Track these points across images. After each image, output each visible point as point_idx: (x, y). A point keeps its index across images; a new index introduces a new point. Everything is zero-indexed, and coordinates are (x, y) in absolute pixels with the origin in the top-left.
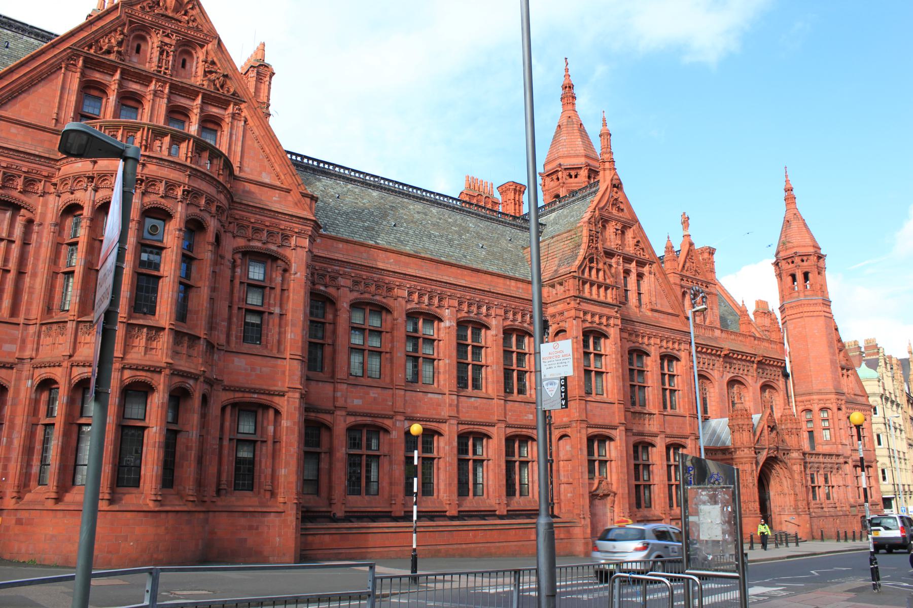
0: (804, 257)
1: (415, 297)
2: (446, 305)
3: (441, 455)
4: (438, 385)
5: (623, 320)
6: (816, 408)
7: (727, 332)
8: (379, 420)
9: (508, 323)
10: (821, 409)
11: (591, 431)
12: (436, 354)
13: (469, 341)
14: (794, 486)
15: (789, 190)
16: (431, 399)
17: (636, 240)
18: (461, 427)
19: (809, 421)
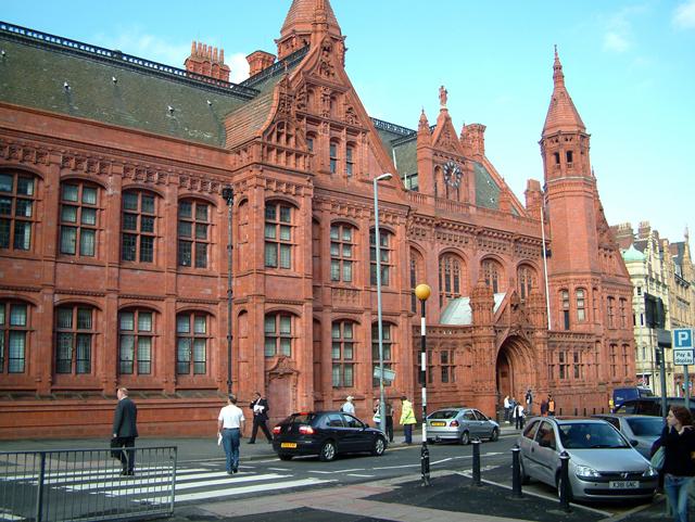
0: (568, 136)
1: (72, 163)
2: (109, 173)
3: (100, 330)
4: (99, 257)
5: (316, 188)
6: (572, 287)
7: (484, 210)
8: (26, 294)
9: (185, 191)
10: (578, 289)
11: (269, 306)
12: (97, 225)
13: (139, 211)
14: (536, 365)
15: (558, 68)
16: (87, 271)
17: (348, 107)
18: (122, 301)
19: (565, 301)
